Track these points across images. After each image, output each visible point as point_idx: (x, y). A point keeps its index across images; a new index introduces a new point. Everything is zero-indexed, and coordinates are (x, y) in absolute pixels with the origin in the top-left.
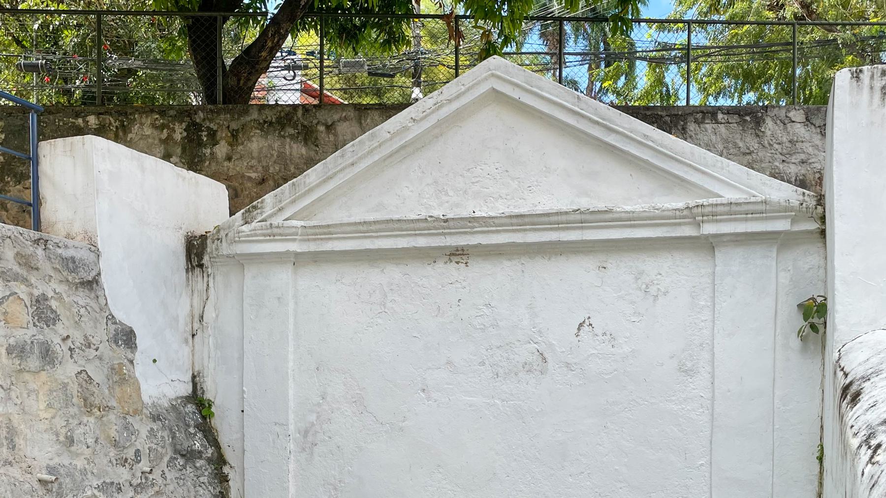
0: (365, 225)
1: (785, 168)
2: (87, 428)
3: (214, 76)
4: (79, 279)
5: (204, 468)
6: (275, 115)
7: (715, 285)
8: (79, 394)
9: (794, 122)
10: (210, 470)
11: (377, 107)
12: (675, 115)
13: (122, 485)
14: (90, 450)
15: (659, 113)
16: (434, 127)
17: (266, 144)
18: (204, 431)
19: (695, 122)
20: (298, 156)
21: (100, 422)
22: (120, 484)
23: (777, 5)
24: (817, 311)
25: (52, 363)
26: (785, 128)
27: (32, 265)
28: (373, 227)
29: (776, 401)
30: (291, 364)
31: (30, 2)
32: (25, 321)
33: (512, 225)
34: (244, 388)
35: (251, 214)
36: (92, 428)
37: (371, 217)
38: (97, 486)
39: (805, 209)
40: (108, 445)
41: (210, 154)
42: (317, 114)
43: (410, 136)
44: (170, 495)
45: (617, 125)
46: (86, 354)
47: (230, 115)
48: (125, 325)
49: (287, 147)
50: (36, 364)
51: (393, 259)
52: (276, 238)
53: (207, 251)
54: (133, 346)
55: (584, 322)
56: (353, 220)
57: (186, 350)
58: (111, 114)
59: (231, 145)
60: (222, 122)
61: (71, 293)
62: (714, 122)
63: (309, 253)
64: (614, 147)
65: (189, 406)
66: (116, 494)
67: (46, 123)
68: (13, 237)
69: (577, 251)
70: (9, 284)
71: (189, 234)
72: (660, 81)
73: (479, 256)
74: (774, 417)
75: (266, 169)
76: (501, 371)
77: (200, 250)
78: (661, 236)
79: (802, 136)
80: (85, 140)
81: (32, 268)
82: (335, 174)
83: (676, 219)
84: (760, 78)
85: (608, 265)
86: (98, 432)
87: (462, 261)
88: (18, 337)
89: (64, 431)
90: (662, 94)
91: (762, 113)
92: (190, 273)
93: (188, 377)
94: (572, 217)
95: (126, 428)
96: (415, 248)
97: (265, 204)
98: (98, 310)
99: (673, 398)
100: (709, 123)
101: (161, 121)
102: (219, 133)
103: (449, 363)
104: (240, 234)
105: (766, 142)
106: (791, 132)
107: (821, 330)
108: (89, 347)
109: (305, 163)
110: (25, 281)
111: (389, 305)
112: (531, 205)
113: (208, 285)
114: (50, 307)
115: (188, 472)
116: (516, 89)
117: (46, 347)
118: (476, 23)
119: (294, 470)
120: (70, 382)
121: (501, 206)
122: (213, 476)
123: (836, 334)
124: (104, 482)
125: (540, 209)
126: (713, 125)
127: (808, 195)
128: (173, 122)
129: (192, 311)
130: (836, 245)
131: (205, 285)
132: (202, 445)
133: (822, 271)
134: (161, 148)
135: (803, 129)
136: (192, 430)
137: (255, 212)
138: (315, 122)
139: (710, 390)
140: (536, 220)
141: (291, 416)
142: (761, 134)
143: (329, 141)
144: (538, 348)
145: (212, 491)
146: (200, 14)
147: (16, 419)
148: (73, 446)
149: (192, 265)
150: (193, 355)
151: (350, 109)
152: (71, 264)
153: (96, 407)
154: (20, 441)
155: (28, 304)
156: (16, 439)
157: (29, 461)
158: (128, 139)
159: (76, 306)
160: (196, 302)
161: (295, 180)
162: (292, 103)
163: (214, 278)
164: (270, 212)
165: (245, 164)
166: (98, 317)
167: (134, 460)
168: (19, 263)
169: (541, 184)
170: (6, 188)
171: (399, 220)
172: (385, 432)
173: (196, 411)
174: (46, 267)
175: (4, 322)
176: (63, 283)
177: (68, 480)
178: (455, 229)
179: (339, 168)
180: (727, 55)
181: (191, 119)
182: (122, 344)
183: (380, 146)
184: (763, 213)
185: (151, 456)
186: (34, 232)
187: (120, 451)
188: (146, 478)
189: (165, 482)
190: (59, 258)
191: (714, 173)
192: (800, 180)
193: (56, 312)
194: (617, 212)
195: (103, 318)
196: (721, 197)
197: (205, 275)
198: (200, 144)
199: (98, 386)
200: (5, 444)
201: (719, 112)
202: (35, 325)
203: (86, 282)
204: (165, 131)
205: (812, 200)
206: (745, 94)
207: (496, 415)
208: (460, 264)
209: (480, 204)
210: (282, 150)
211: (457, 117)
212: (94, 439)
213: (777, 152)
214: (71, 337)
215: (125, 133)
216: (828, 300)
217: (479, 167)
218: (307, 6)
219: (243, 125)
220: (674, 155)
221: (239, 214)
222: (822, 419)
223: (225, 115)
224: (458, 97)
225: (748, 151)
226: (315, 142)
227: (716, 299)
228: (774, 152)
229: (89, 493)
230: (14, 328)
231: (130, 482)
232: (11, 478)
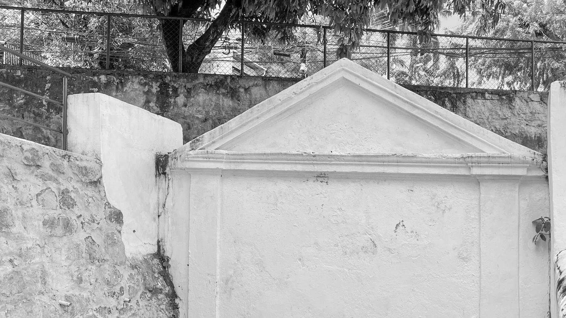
0: (265, 156)
1: (528, 129)
2: (91, 272)
3: (177, 54)
4: (89, 180)
5: (163, 300)
7: (480, 206)
8: (87, 251)
9: (533, 101)
10: (167, 301)
12: (459, 93)
15: (449, 91)
20: (227, 106)
21: (99, 269)
22: (110, 308)
24: (545, 227)
25: (71, 231)
26: (528, 105)
27: (60, 171)
28: (270, 157)
29: (520, 282)
30: (218, 238)
31: (71, 1)
32: (55, 205)
33: (355, 161)
34: (189, 251)
35: (196, 144)
37: (268, 151)
38: (96, 309)
40: (104, 283)
42: (239, 81)
43: (293, 103)
44: (142, 316)
45: (419, 104)
46: (92, 226)
47: (186, 79)
48: (116, 209)
49: (221, 100)
50: (61, 232)
52: (210, 160)
53: (168, 165)
54: (121, 222)
55: (399, 223)
56: (257, 152)
57: (154, 225)
58: (114, 75)
60: (181, 83)
61: (84, 188)
63: (231, 170)
64: (417, 117)
65: (155, 260)
66: (107, 315)
67: (76, 78)
68: (49, 153)
69: (395, 180)
70: (46, 182)
71: (158, 153)
72: (452, 66)
75: (208, 113)
76: (348, 251)
77: (164, 163)
79: (538, 110)
80: (95, 96)
82: (247, 123)
83: (455, 164)
84: (515, 67)
85: (414, 189)
86: (97, 275)
87: (324, 181)
88: (50, 215)
89: (76, 274)
91: (513, 95)
92: (158, 178)
94: (391, 159)
95: (115, 273)
96: (296, 171)
97: (204, 139)
98: (100, 200)
99: (455, 275)
101: (145, 81)
102: (179, 90)
103: (316, 243)
104: (189, 156)
105: (516, 112)
107: (547, 238)
108: (94, 222)
109: (231, 111)
110: (56, 180)
113: (169, 186)
114: (71, 197)
115: (153, 302)
116: (357, 79)
117: (67, 222)
118: (335, 32)
120: (81, 244)
123: (555, 245)
125: (372, 153)
128: (152, 81)
129: (158, 201)
130: (553, 189)
131: (167, 185)
132: (162, 285)
133: (547, 201)
135: (539, 106)
136: (156, 275)
137: (198, 143)
138: (238, 86)
139: (478, 271)
140: (369, 159)
141: (218, 270)
142: (512, 107)
143: (246, 98)
144: (371, 238)
145: (168, 315)
146: (170, 18)
147: (47, 266)
148: (82, 283)
149: (159, 173)
150: (158, 228)
151: (259, 79)
152: (84, 171)
154: (49, 280)
156: (47, 278)
157: (54, 292)
158: (124, 91)
159: (86, 196)
160: (161, 196)
161: (222, 125)
162: (224, 74)
163: (172, 182)
164: (207, 144)
165: (195, 109)
166: (100, 204)
167: (119, 294)
169: (372, 137)
170: (50, 116)
172: (276, 284)
173: (160, 263)
174: (69, 173)
176: (79, 182)
177: (78, 305)
179: (249, 119)
180: (494, 53)
181: (163, 80)
182: (114, 221)
183: (274, 108)
184: (509, 164)
185: (130, 291)
186: (63, 150)
188: (127, 305)
190: (77, 167)
193: (74, 200)
194: (419, 157)
195: (103, 204)
196: (483, 152)
197: (167, 179)
198: (168, 96)
200: (40, 281)
201: (486, 92)
204: (147, 87)
206: (506, 77)
210: (217, 102)
211: (321, 93)
212: (95, 280)
213: (523, 119)
215: (123, 87)
219: (194, 86)
220: (454, 124)
221: (188, 144)
222: (549, 295)
223: (183, 79)
225: (504, 117)
228: (521, 119)
229: (91, 313)
230: (48, 209)
232: (43, 303)
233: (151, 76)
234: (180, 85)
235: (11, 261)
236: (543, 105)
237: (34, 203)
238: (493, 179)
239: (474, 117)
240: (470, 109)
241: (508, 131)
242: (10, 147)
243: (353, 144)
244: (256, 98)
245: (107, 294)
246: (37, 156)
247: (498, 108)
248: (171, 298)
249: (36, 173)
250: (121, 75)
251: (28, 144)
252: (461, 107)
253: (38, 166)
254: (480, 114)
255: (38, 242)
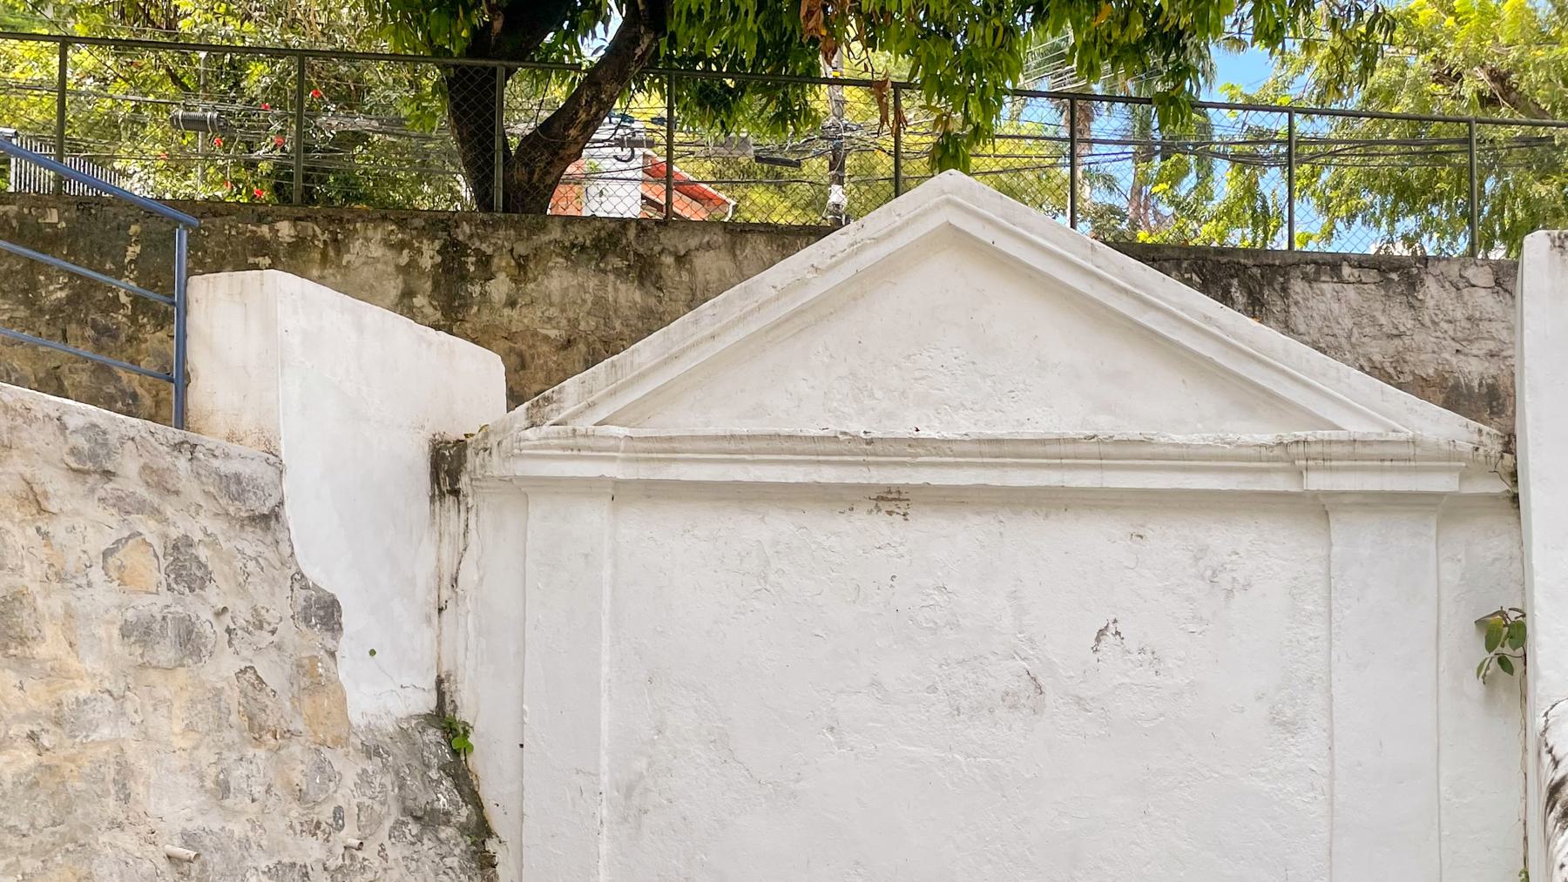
0: (732, 442)
1: (1461, 364)
2: (253, 767)
3: (490, 163)
4: (247, 511)
6: (590, 234)
7: (1330, 578)
8: (241, 709)
9: (1474, 286)
10: (463, 846)
11: (762, 229)
12: (1269, 265)
13: (309, 869)
14: (256, 807)
15: (1242, 261)
16: (850, 282)
17: (575, 282)
18: (454, 777)
19: (1302, 279)
21: (275, 757)
22: (305, 866)
23: (1449, 74)
24: (1510, 636)
25: (197, 653)
26: (1460, 297)
27: (169, 486)
28: (747, 446)
29: (1443, 788)
30: (605, 669)
33: (982, 455)
34: (525, 707)
35: (542, 410)
36: (261, 767)
37: (742, 429)
39: (1483, 458)
41: (481, 293)
42: (661, 235)
43: (811, 294)
45: (1158, 297)
46: (255, 639)
48: (323, 590)
49: (610, 289)
51: (779, 499)
54: (336, 626)
55: (1107, 627)
56: (712, 430)
57: (428, 635)
58: (315, 220)
59: (514, 280)
60: (502, 242)
62: (1335, 280)
64: (1154, 332)
65: (431, 731)
68: (138, 438)
72: (1251, 191)
73: (926, 503)
74: (1439, 814)
75: (573, 323)
76: (964, 704)
78: (1235, 488)
79: (1489, 309)
81: (168, 491)
82: (684, 351)
83: (1261, 461)
84: (1424, 193)
86: (271, 774)
87: (897, 510)
89: (213, 771)
90: (1255, 211)
91: (1418, 268)
92: (438, 503)
93: (430, 682)
94: (1083, 448)
96: (819, 485)
97: (564, 395)
98: (278, 565)
99: (1263, 770)
100: (1328, 282)
101: (400, 236)
102: (496, 260)
103: (875, 683)
104: (522, 444)
105: (1427, 318)
106: (1470, 304)
107: (1518, 671)
108: (261, 628)
110: (156, 512)
111: (772, 577)
112: (1015, 423)
113: (467, 526)
114: (197, 557)
115: (425, 847)
116: (988, 227)
117: (187, 627)
119: (607, 854)
120: (227, 688)
121: (963, 421)
122: (468, 857)
123: (1540, 685)
124: (280, 862)
125: (1029, 432)
126: (1335, 285)
127: (1488, 433)
129: (438, 568)
132: (450, 801)
133: (1516, 565)
134: (398, 281)
136: (434, 774)
138: (657, 249)
140: (1022, 449)
141: (605, 761)
142: (1417, 304)
143: (681, 282)
144: (1028, 668)
147: (132, 750)
149: (440, 490)
151: (717, 230)
152: (234, 487)
153: (269, 730)
154: (137, 789)
155: (160, 553)
156: (131, 784)
157: (153, 823)
158: (344, 263)
159: (239, 556)
160: (447, 553)
161: (615, 357)
162: (619, 216)
165: (539, 314)
167: (331, 826)
168: (147, 483)
171: (790, 437)
173: (443, 741)
174: (192, 490)
175: (117, 582)
177: (217, 857)
178: (886, 456)
180: (1365, 155)
181: (449, 235)
182: (316, 624)
184: (1410, 460)
185: (362, 818)
187: (308, 808)
188: (353, 858)
189: (385, 865)
190: (213, 475)
191: (1325, 388)
192: (1487, 384)
193: (206, 567)
195: (286, 578)
196: (1337, 428)
197: (462, 508)
198: (464, 277)
199: (274, 696)
200: (113, 792)
201: (1345, 263)
202: (170, 589)
203: (258, 517)
204: (406, 252)
205: (1496, 442)
206: (1398, 220)
207: (956, 780)
208: (894, 515)
209: (928, 416)
211: (888, 269)
212: (266, 787)
213: (1446, 336)
214: (230, 610)
215: (338, 253)
216: (1528, 616)
217: (925, 354)
218: (647, 57)
222: (1525, 824)
224: (891, 234)
225: (1395, 332)
226: (657, 283)
227: (1333, 602)
228: (1442, 336)
230: (135, 592)
231: (324, 864)
233: (419, 222)
234: (498, 248)
235: (32, 736)
236: (1501, 298)
237: (96, 574)
238: (1367, 504)
239: (1311, 332)
240: (1299, 308)
241: (1406, 369)
242: (30, 421)
243: (976, 407)
244: (708, 283)
245: (298, 828)
246: (105, 444)
247: (1378, 305)
248: (474, 838)
249: (101, 493)
250: (334, 220)
251: (80, 413)
252: (1275, 305)
253: (108, 475)
254: (1327, 323)
255: (107, 685)
